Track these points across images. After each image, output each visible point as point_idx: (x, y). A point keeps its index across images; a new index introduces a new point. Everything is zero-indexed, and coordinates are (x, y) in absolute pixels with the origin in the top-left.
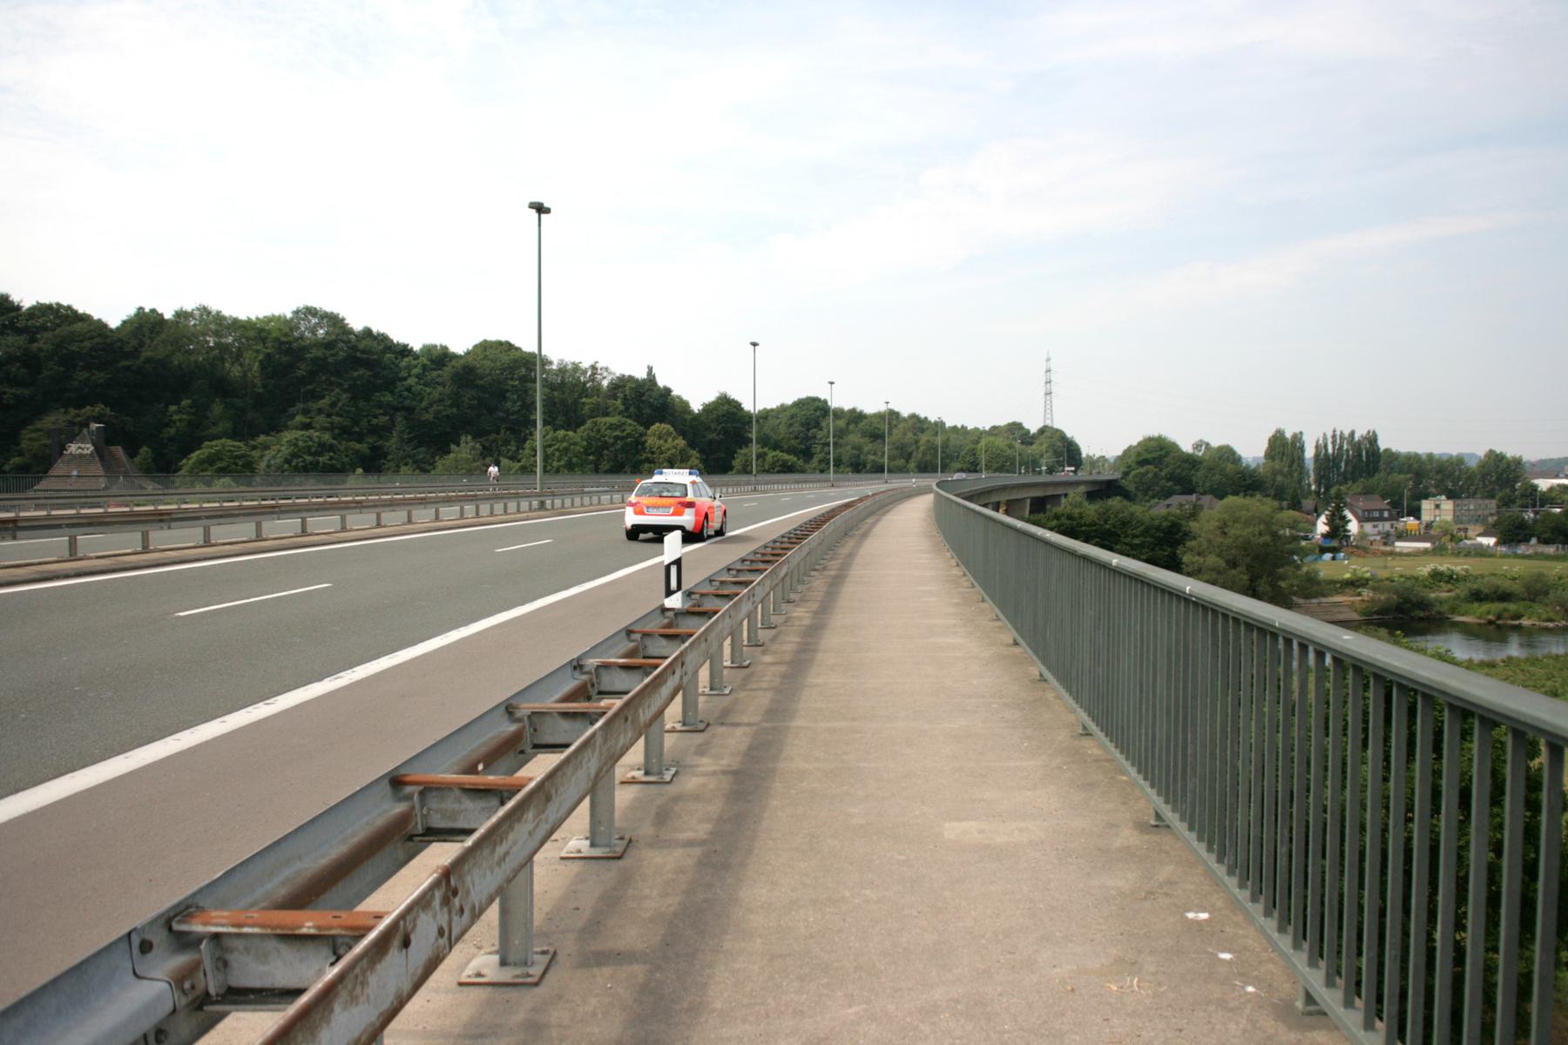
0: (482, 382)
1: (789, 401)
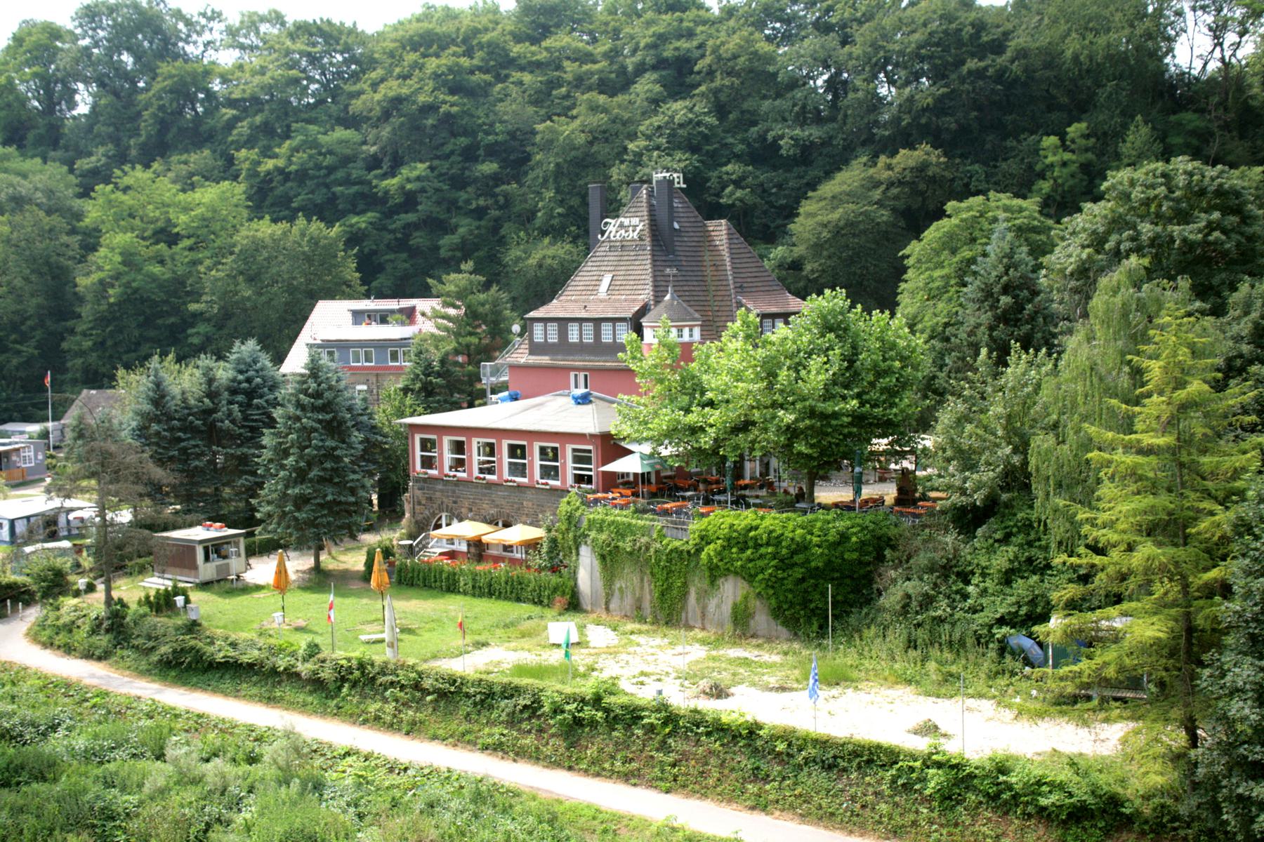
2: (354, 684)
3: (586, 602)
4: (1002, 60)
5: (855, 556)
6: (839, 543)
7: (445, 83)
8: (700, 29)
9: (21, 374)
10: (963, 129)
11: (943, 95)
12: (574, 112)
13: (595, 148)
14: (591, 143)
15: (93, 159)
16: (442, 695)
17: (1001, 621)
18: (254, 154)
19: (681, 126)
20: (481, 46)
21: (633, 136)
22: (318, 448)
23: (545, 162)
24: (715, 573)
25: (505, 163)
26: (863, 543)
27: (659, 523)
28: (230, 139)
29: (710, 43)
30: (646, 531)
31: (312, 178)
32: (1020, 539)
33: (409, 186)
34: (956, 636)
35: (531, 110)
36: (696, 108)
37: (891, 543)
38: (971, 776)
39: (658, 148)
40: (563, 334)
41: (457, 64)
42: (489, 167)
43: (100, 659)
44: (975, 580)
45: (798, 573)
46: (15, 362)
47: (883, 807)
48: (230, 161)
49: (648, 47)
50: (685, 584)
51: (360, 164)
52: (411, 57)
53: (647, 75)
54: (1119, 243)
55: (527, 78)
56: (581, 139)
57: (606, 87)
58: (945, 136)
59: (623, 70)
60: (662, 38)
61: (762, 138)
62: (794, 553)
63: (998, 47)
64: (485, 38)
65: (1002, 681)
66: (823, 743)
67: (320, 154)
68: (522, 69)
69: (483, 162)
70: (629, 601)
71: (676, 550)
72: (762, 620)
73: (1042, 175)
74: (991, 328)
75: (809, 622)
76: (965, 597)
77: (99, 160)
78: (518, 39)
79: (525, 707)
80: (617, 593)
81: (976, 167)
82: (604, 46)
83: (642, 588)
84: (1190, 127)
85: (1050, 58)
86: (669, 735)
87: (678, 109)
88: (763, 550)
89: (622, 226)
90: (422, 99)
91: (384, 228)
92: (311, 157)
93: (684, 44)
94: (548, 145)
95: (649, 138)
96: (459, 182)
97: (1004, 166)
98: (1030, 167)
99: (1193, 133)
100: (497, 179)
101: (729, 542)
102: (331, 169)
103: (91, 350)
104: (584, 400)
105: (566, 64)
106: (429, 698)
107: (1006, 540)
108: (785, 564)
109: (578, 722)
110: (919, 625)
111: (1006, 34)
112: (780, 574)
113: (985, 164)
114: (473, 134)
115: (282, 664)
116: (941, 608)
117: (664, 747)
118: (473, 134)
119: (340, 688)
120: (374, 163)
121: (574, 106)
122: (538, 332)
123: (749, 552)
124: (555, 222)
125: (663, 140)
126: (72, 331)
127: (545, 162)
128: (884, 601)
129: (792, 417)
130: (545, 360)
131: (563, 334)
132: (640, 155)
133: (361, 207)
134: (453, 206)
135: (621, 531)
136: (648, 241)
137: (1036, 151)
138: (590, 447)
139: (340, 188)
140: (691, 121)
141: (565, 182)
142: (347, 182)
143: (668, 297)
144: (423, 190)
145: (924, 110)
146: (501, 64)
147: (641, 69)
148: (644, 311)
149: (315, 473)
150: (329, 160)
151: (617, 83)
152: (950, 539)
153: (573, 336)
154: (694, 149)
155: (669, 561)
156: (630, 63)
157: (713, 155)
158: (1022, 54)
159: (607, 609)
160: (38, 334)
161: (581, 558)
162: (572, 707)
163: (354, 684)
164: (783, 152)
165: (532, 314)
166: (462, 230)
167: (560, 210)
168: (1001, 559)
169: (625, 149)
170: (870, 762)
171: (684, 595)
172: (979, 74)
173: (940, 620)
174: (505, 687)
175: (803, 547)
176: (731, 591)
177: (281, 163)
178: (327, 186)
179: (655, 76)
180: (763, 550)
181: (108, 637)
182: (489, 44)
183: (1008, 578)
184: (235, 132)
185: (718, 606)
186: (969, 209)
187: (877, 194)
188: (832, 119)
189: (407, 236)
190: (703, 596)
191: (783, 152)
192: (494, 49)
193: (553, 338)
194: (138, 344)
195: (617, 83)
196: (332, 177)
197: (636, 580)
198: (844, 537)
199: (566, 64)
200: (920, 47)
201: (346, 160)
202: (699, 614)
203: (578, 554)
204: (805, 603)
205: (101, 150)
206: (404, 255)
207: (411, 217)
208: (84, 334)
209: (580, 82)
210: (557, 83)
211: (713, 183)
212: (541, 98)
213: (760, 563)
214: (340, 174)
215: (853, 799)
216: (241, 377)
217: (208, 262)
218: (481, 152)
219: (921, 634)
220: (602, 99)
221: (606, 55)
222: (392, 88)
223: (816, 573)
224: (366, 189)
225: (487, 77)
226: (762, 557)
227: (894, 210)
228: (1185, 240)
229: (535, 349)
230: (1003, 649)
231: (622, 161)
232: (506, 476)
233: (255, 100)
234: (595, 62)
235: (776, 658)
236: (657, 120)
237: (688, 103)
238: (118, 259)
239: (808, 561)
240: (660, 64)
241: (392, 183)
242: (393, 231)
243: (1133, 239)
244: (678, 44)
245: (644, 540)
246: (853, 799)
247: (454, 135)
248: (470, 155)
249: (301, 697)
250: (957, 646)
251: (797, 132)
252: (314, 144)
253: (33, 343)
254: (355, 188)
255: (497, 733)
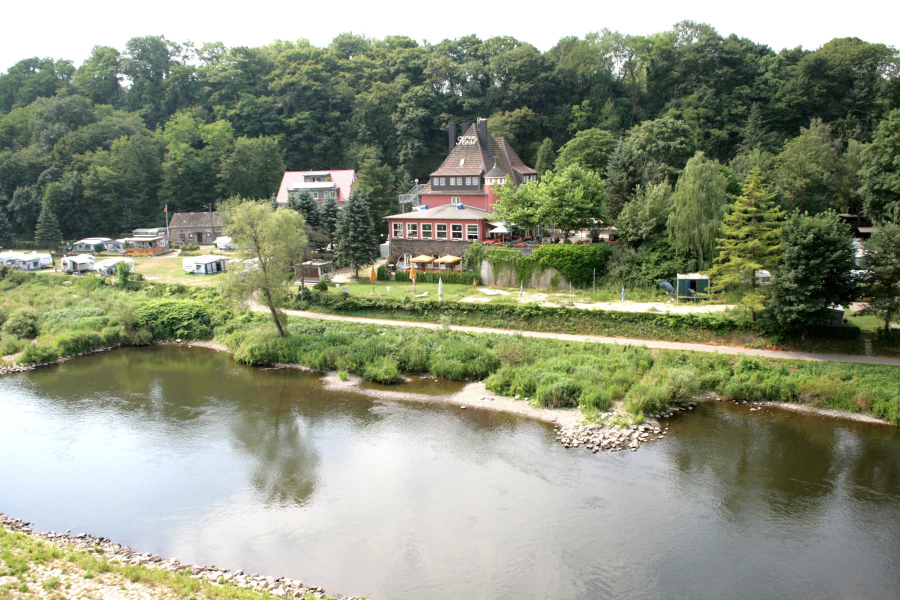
0: (832, 73)
1: (828, 42)
2: (429, 310)
3: (486, 281)
4: (554, 73)
5: (599, 258)
6: (593, 254)
7: (312, 77)
8: (422, 55)
9: (140, 207)
10: (540, 101)
11: (532, 87)
12: (371, 90)
13: (382, 106)
14: (380, 104)
15: (144, 110)
16: (470, 311)
17: (657, 277)
18: (223, 107)
19: (420, 97)
20: (322, 60)
21: (400, 101)
22: (361, 228)
23: (360, 112)
24: (544, 266)
25: (342, 112)
26: (601, 254)
27: (519, 251)
28: (210, 100)
29: (429, 62)
30: (513, 254)
31: (252, 118)
32: (660, 249)
33: (301, 122)
34: (641, 283)
35: (350, 88)
36: (426, 89)
37: (610, 253)
38: (683, 319)
39: (411, 106)
40: (464, 182)
41: (316, 68)
42: (337, 114)
43: (304, 310)
44: (644, 264)
45: (579, 265)
46: (138, 201)
47: (655, 331)
48: (211, 110)
49: (401, 62)
50: (531, 272)
51: (274, 112)
52: (293, 65)
53: (401, 75)
54: (651, 148)
55: (347, 75)
56: (376, 102)
57: (382, 79)
58: (532, 104)
59: (388, 72)
60: (406, 59)
61: (455, 102)
62: (577, 258)
63: (551, 68)
64: (325, 56)
65: (660, 297)
66: (629, 314)
67: (256, 107)
68: (343, 70)
69: (332, 112)
70: (505, 280)
71: (528, 260)
72: (563, 283)
73: (572, 121)
74: (627, 178)
75: (582, 283)
76: (641, 271)
77: (147, 111)
78: (340, 57)
79: (507, 312)
80: (500, 278)
81: (545, 117)
82: (378, 62)
83: (511, 275)
84: (625, 103)
85: (572, 74)
86: (569, 317)
87: (418, 89)
88: (566, 258)
89: (467, 139)
90: (304, 83)
91: (287, 141)
92: (252, 109)
93: (418, 62)
94: (361, 104)
95: (406, 102)
96: (321, 120)
97: (557, 117)
98: (567, 118)
99: (626, 106)
100: (338, 119)
101: (552, 255)
102: (262, 114)
103: (171, 195)
104: (462, 208)
105: (365, 69)
106: (465, 312)
107: (653, 250)
108: (574, 262)
109: (531, 315)
110: (626, 281)
111: (553, 63)
112: (572, 266)
113: (549, 116)
114: (327, 99)
115: (395, 305)
116: (634, 274)
117: (567, 320)
118: (327, 99)
119: (423, 313)
120: (280, 111)
121: (370, 87)
122: (436, 182)
123: (560, 259)
124: (367, 138)
125: (413, 103)
126: (160, 187)
127: (360, 112)
128: (611, 273)
129: (572, 210)
130: (440, 192)
131: (448, 182)
132: (404, 109)
133: (276, 131)
134: (318, 130)
135: (503, 254)
136: (479, 145)
137: (569, 111)
138: (477, 225)
139: (267, 123)
140: (424, 95)
141: (369, 120)
142: (270, 120)
143: (494, 167)
144: (307, 124)
145: (524, 93)
146: (333, 68)
147: (397, 72)
148: (483, 173)
149: (361, 238)
150: (261, 110)
151: (389, 78)
152: (632, 251)
153: (452, 182)
154: (426, 106)
155: (525, 264)
156: (392, 69)
157: (434, 109)
158: (560, 71)
159: (496, 284)
160: (146, 189)
161: (482, 266)
162: (528, 310)
163: (429, 310)
164: (465, 109)
165: (432, 174)
166: (324, 141)
167: (368, 133)
168: (654, 257)
169: (397, 106)
170: (645, 319)
171: (530, 276)
172: (546, 79)
173: (634, 279)
174: (497, 306)
175: (581, 256)
176: (550, 274)
177: (238, 112)
178: (259, 121)
179: (405, 75)
180: (566, 258)
181: (305, 301)
182: (326, 59)
183: (657, 263)
184: (212, 97)
185: (545, 280)
186: (587, 134)
187: (508, 127)
188: (484, 95)
189: (298, 144)
190: (538, 276)
191: (465, 109)
192: (329, 61)
193: (443, 184)
194: (191, 193)
195: (389, 78)
196: (263, 118)
197: (509, 272)
198: (595, 252)
199: (365, 69)
200: (521, 67)
201: (268, 111)
202: (536, 282)
203: (481, 264)
204: (581, 276)
205: (148, 106)
206: (297, 153)
207: (300, 136)
208: (168, 188)
209: (371, 77)
210: (361, 77)
211: (436, 122)
212: (353, 84)
213: (566, 262)
214: (266, 116)
215: (643, 330)
216: (304, 202)
217: (224, 156)
218: (330, 107)
219: (629, 283)
220: (384, 84)
221: (381, 66)
222: (287, 79)
223: (586, 265)
224: (278, 123)
225: (329, 74)
226: (566, 260)
227: (515, 134)
228: (675, 148)
229: (434, 188)
230: (658, 287)
231: (396, 112)
232: (436, 237)
233: (220, 83)
234: (376, 68)
235: (574, 296)
236: (409, 94)
237: (422, 87)
238: (183, 154)
239: (582, 261)
240: (408, 70)
241: (292, 120)
242: (292, 142)
243: (656, 146)
244: (415, 62)
245: (513, 257)
246: (643, 330)
247: (319, 99)
248: (325, 108)
249: (407, 317)
250: (642, 286)
251: (470, 100)
252: (253, 103)
253: (144, 193)
254: (273, 123)
255: (499, 321)
